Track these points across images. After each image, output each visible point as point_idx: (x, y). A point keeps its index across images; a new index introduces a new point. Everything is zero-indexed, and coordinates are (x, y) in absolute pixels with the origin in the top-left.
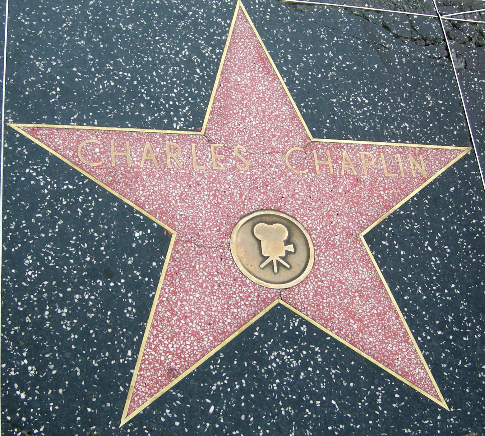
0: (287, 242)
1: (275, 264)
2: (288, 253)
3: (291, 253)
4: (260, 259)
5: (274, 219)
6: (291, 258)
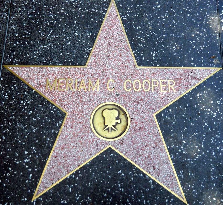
0: (117, 118)
2: (117, 123)
3: (118, 123)
5: (111, 107)
6: (118, 126)
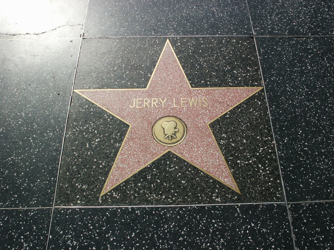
0: (175, 128)
1: (170, 137)
2: (176, 132)
3: (177, 132)
4: (164, 135)
6: (177, 134)
